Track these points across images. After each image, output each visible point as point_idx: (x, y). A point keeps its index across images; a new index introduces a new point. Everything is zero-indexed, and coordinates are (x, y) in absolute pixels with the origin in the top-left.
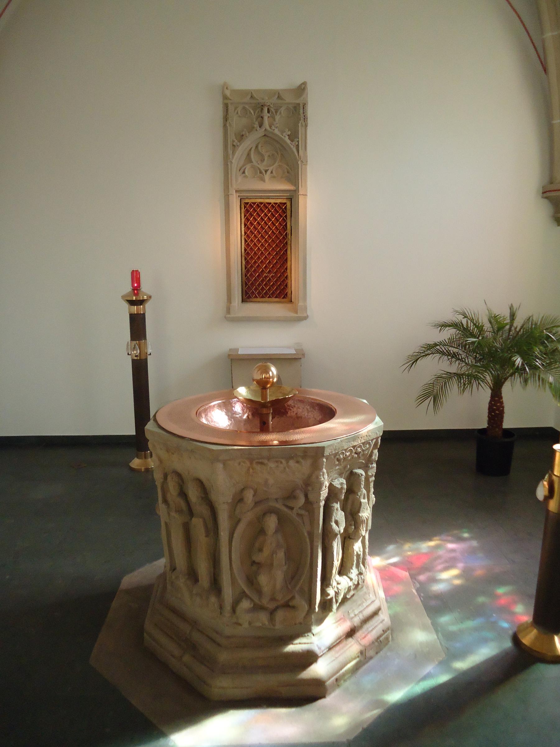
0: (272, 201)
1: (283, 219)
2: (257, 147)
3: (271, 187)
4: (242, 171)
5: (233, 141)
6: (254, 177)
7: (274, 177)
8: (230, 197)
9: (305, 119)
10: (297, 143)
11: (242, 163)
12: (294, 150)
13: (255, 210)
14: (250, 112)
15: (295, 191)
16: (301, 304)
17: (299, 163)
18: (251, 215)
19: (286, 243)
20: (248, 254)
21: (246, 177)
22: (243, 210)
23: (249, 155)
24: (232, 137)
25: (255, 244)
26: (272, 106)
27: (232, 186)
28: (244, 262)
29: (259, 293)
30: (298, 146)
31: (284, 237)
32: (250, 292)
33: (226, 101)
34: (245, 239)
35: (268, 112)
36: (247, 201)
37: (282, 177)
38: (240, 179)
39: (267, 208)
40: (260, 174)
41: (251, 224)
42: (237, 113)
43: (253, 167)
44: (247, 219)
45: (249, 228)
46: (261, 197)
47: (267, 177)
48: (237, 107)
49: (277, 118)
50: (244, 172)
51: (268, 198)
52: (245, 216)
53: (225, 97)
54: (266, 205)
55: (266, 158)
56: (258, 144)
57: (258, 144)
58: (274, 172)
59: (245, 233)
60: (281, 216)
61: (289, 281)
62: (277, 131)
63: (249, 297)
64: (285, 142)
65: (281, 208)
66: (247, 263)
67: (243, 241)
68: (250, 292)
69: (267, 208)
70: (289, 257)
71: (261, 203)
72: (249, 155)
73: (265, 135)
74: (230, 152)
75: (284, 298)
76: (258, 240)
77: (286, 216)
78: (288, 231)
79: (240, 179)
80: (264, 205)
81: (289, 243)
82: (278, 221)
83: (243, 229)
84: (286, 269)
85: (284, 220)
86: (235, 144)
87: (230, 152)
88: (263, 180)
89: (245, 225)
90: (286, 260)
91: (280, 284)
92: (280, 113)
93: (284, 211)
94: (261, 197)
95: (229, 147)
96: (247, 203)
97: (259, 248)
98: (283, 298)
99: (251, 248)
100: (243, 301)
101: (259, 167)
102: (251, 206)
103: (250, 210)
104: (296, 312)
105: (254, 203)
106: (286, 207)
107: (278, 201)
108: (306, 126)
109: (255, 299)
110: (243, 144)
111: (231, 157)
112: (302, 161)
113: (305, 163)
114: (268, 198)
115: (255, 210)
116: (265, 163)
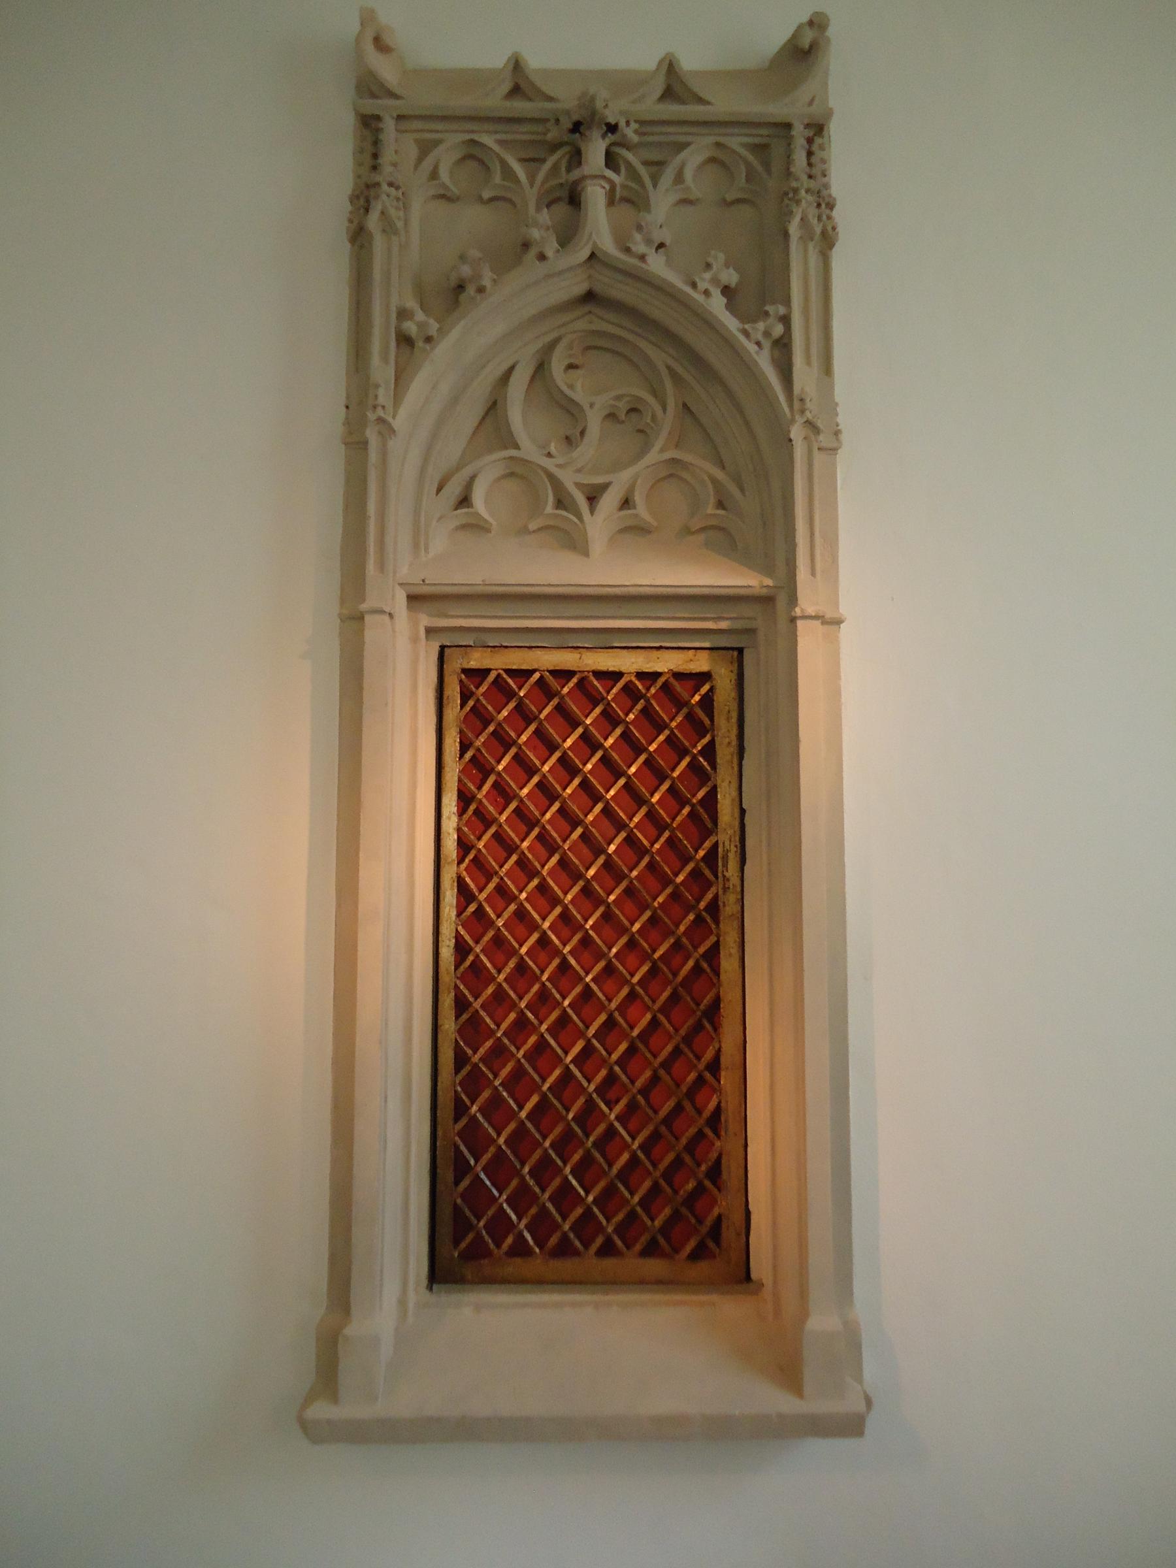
0: (629, 663)
1: (694, 766)
2: (541, 368)
3: (625, 576)
4: (454, 489)
5: (403, 314)
6: (524, 531)
7: (640, 530)
8: (374, 631)
9: (825, 204)
10: (779, 330)
11: (453, 447)
12: (764, 362)
13: (524, 715)
14: (504, 164)
15: (766, 600)
16: (821, 1321)
17: (797, 433)
18: (502, 741)
19: (714, 908)
20: (475, 975)
21: (477, 527)
22: (453, 713)
23: (494, 408)
24: (393, 294)
25: (521, 914)
26: (630, 133)
27: (381, 566)
28: (449, 1025)
29: (542, 1226)
30: (782, 346)
31: (696, 874)
32: (486, 1224)
33: (370, 106)
34: (460, 882)
35: (611, 160)
36: (476, 661)
37: (687, 531)
38: (439, 543)
39: (595, 700)
40: (560, 512)
41: (503, 793)
42: (434, 175)
43: (518, 471)
44: (478, 768)
45: (484, 820)
46: (562, 638)
47: (599, 525)
48: (436, 143)
49: (662, 201)
50: (465, 501)
51: (606, 640)
52: (464, 747)
53: (369, 86)
54: (588, 688)
55: (594, 422)
56: (552, 346)
57: (552, 346)
58: (638, 498)
59: (464, 846)
60: (683, 752)
61: (727, 1144)
62: (657, 265)
63: (477, 1252)
64: (708, 323)
65: (680, 704)
66: (472, 1029)
67: (450, 896)
68: (486, 1224)
69: (595, 700)
70: (730, 995)
71: (564, 675)
72: (494, 408)
73: (590, 297)
74: (382, 370)
75: (698, 1254)
76: (543, 888)
77: (710, 752)
78: (725, 836)
79: (439, 543)
80: (582, 684)
81: (729, 906)
82: (661, 777)
83: (450, 823)
84: (715, 1067)
85: (699, 774)
86: (411, 328)
87: (382, 370)
88: (576, 544)
89: (465, 800)
90: (714, 1011)
91: (678, 1162)
92: (679, 178)
93: (700, 722)
94: (562, 638)
95: (381, 340)
96: (479, 674)
97: (543, 941)
98: (695, 1256)
99: (498, 941)
100: (440, 1274)
101: (559, 474)
102: (501, 690)
103: (501, 716)
104: (789, 1373)
105: (522, 675)
106: (707, 702)
107: (665, 663)
108: (828, 240)
109: (517, 1266)
110: (455, 333)
111: (384, 396)
112: (809, 423)
113: (825, 436)
114: (606, 640)
115: (524, 715)
116: (587, 451)
